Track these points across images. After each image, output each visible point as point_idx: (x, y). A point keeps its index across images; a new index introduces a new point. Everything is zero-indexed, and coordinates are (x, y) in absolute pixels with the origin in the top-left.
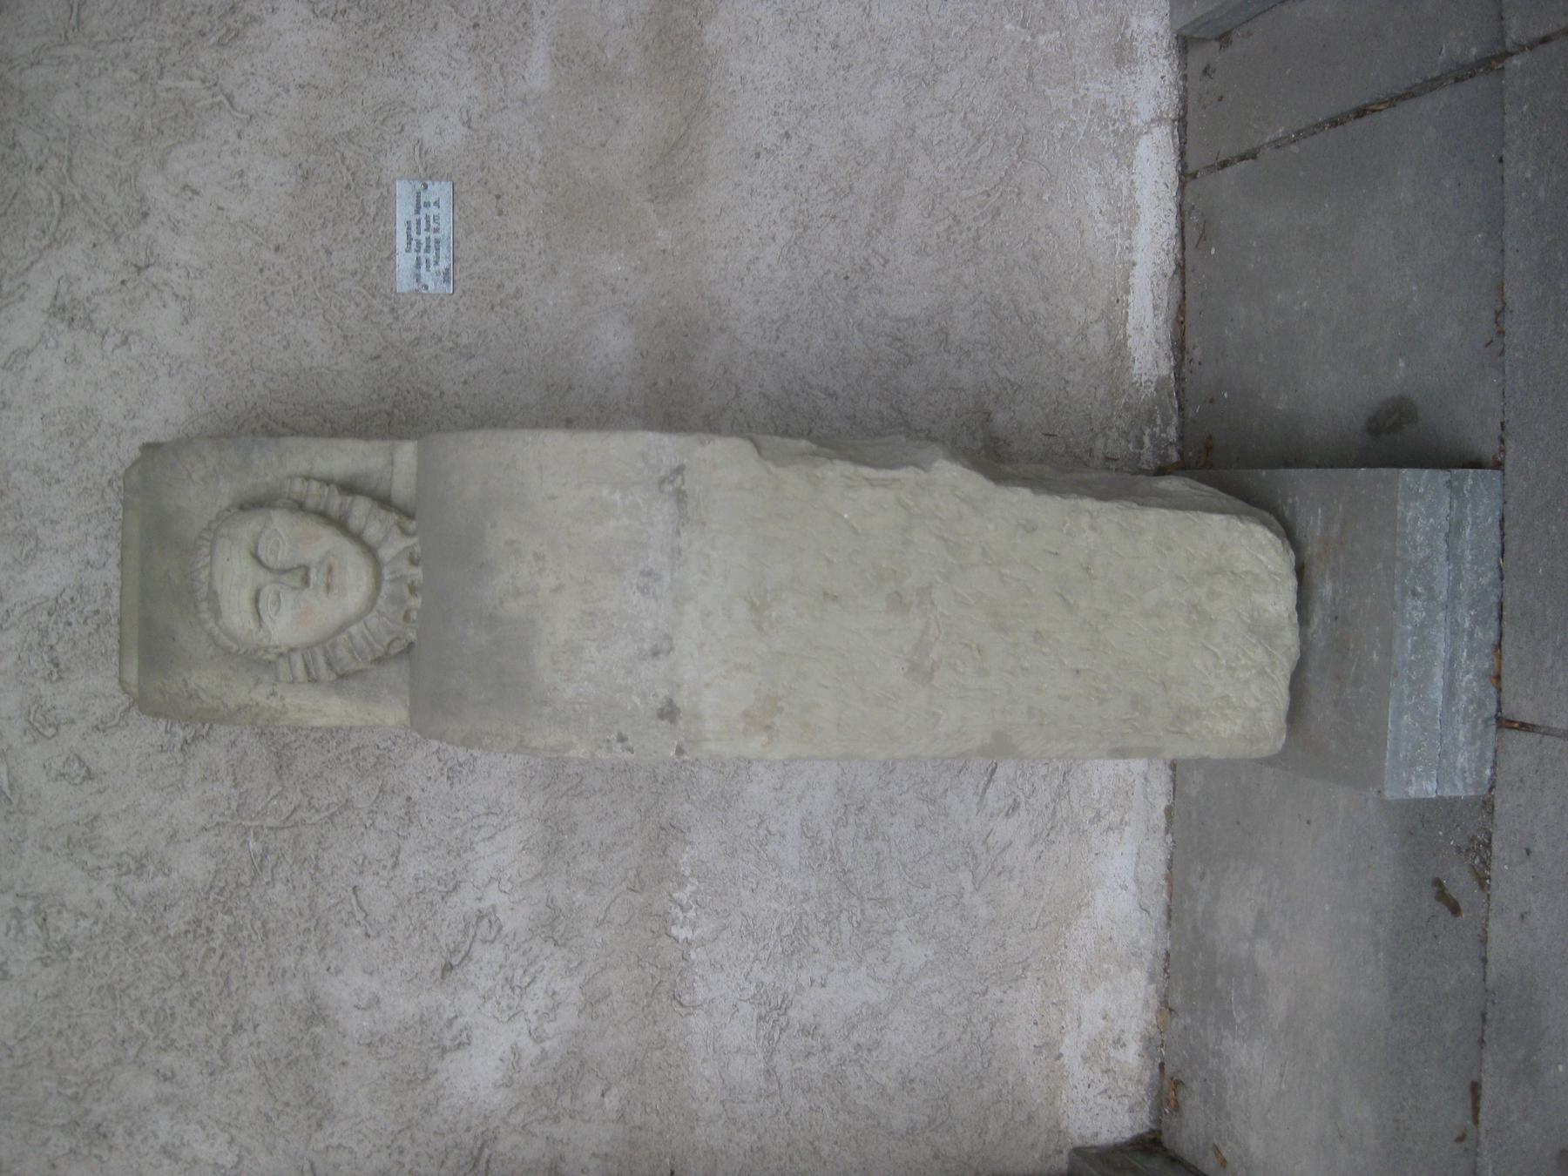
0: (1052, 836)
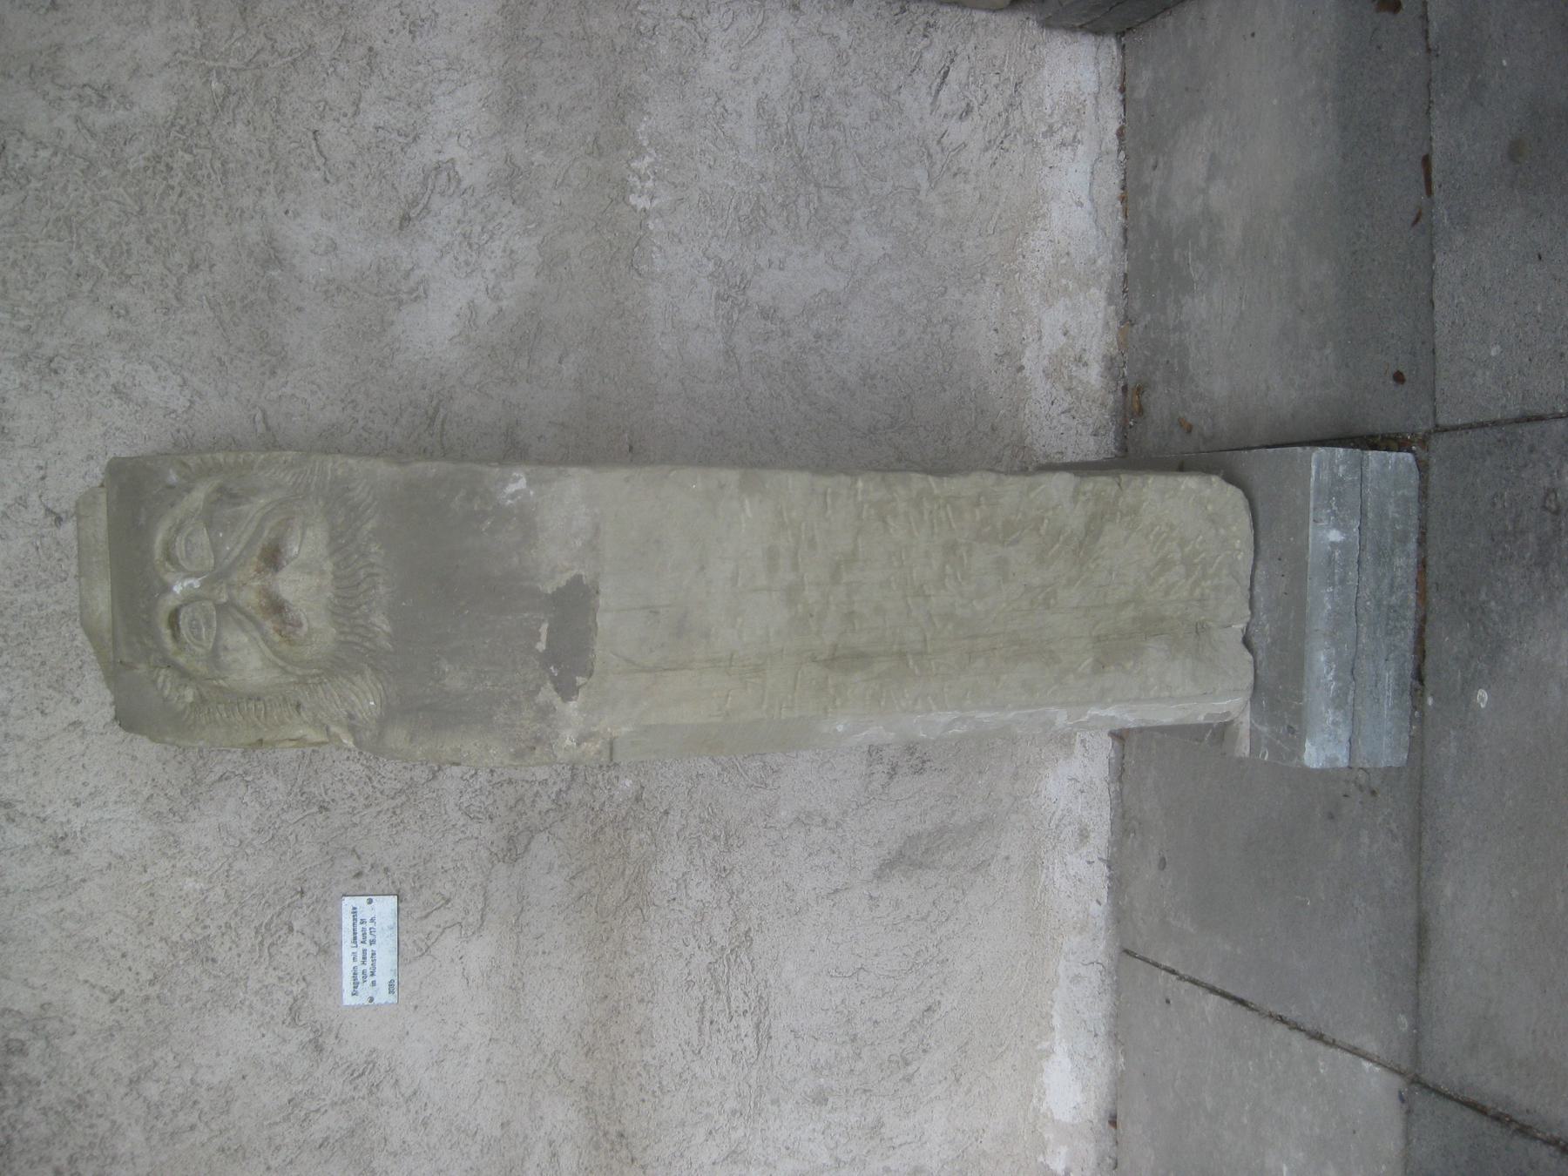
0: (1006, 145)
